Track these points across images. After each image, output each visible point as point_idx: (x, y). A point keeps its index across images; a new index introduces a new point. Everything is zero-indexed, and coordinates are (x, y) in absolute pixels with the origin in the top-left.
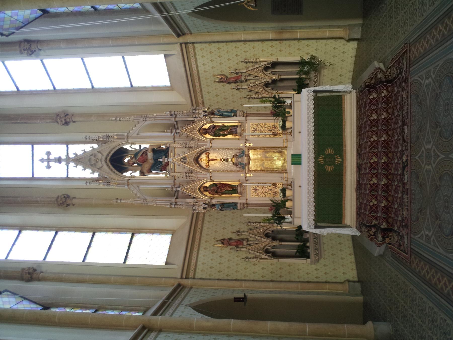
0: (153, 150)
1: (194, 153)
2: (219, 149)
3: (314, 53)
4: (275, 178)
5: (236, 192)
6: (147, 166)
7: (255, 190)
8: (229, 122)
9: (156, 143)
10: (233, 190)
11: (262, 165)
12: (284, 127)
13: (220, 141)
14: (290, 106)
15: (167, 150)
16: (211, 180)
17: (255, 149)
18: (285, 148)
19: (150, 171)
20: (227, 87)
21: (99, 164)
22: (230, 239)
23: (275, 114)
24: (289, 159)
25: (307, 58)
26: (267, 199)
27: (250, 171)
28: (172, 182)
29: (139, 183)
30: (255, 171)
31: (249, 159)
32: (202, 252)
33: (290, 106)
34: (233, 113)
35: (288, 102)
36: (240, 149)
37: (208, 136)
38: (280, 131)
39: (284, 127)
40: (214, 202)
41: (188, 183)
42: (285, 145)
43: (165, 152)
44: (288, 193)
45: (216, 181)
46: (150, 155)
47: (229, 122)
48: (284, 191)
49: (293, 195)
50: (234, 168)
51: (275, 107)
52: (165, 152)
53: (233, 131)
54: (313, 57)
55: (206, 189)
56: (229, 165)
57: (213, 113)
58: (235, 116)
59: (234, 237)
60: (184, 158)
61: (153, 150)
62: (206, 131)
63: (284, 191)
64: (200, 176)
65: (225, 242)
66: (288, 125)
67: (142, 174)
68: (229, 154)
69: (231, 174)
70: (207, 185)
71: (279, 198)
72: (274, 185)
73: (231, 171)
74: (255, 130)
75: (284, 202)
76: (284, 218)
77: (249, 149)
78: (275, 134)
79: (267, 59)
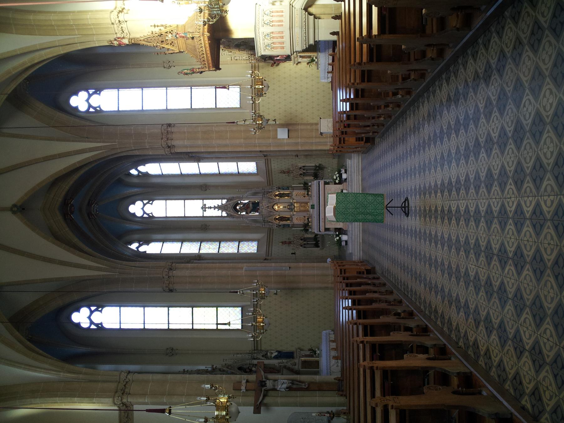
0: (252, 203)
1: (272, 204)
2: (282, 203)
3: (320, 163)
4: (305, 214)
5: (289, 220)
6: (249, 210)
7: (297, 219)
8: (286, 192)
9: (252, 200)
10: (288, 219)
11: (300, 209)
12: (308, 194)
13: (282, 199)
14: (310, 186)
15: (258, 203)
16: (279, 215)
17: (297, 203)
18: (309, 202)
19: (250, 212)
20: (284, 175)
21: (229, 209)
22: (285, 241)
23: (304, 189)
24: (310, 206)
25: (317, 165)
26: (301, 222)
27: (295, 212)
28: (261, 216)
29: (247, 218)
30: (296, 212)
31: (295, 207)
32: (273, 247)
33: (310, 186)
34: (288, 188)
35: (310, 184)
36: (291, 202)
37: (277, 197)
38: (306, 196)
39: (308, 194)
40: (280, 224)
41: (270, 216)
42: (308, 201)
43: (258, 204)
44: (310, 220)
45: (281, 216)
46: (251, 205)
47: (286, 192)
48: (308, 219)
49: (312, 225)
50: (288, 210)
51: (304, 186)
52: (258, 204)
53: (288, 195)
54: (320, 165)
55: (277, 219)
56: (286, 209)
57: (279, 188)
58: (289, 189)
59: (287, 241)
60: (268, 206)
61: (252, 203)
62: (276, 195)
63: (308, 219)
64: (275, 214)
65: (284, 243)
66: (309, 193)
67: (247, 213)
68: (286, 205)
69: (287, 213)
70: (277, 217)
71: (306, 222)
72: (304, 217)
73: (287, 212)
74: (297, 195)
75: (308, 224)
76: (308, 230)
77: (294, 202)
78: (304, 197)
79: (300, 165)
